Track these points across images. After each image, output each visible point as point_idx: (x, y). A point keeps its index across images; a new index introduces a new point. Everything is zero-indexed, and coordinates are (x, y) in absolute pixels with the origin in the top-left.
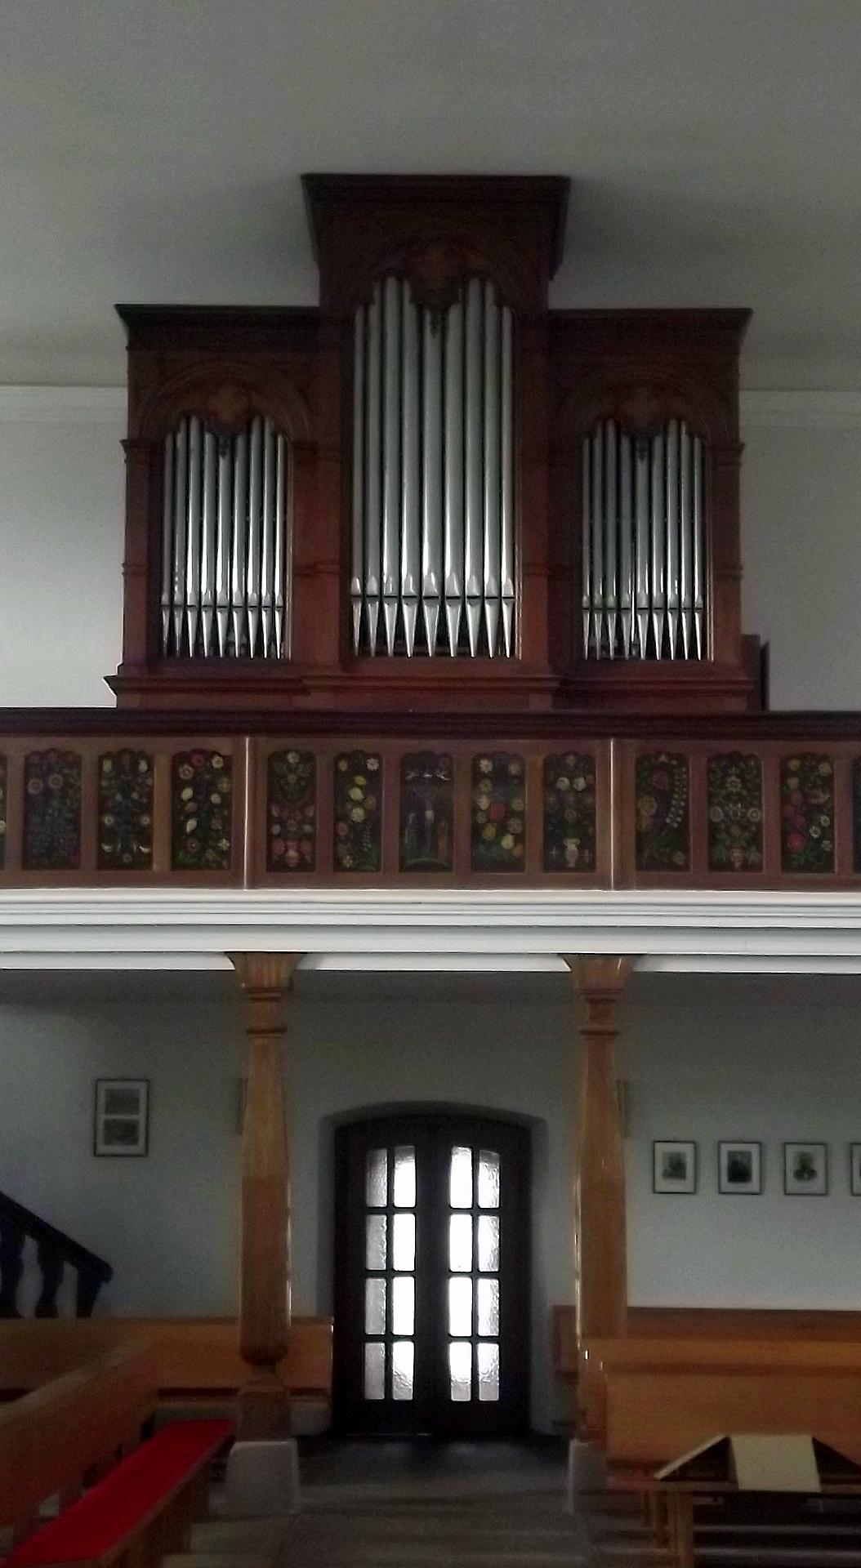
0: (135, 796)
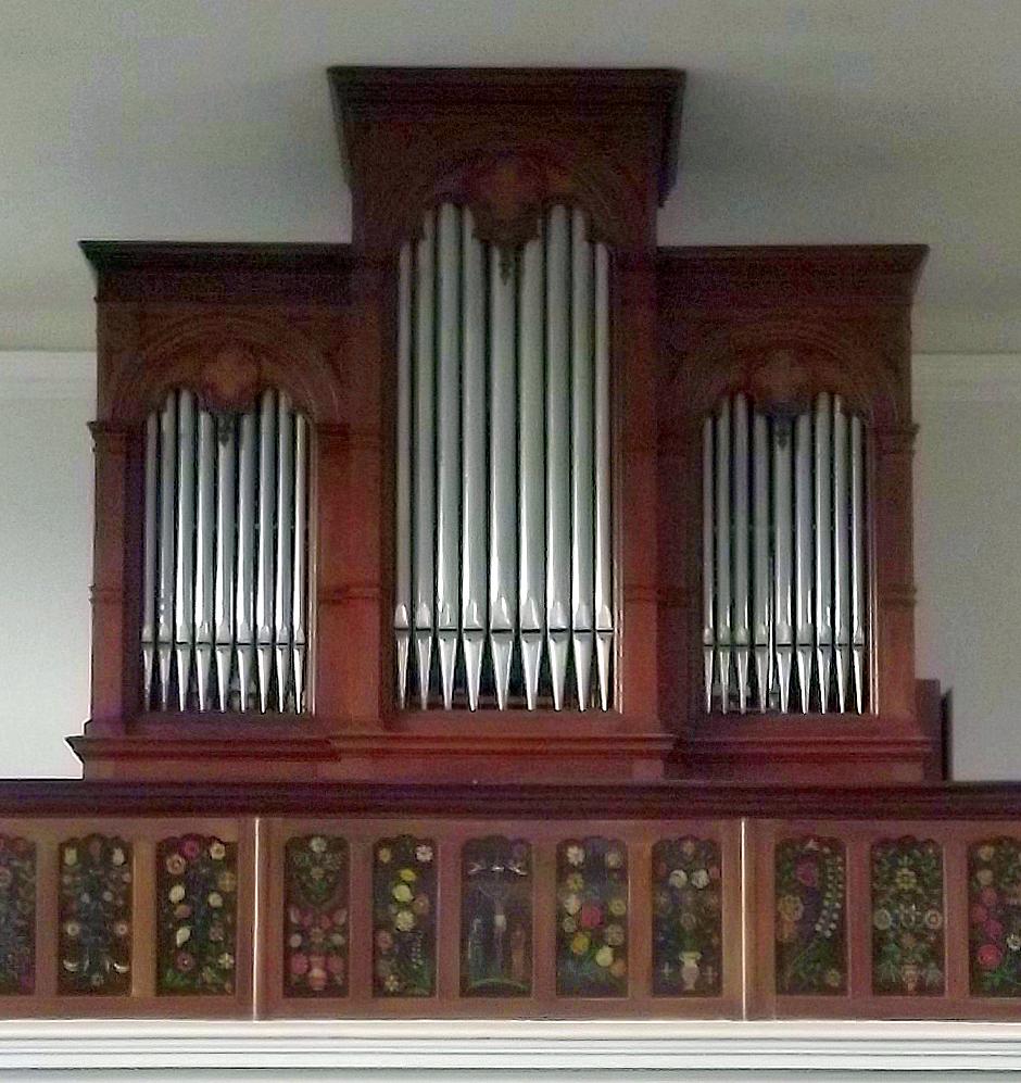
0: (107, 896)
